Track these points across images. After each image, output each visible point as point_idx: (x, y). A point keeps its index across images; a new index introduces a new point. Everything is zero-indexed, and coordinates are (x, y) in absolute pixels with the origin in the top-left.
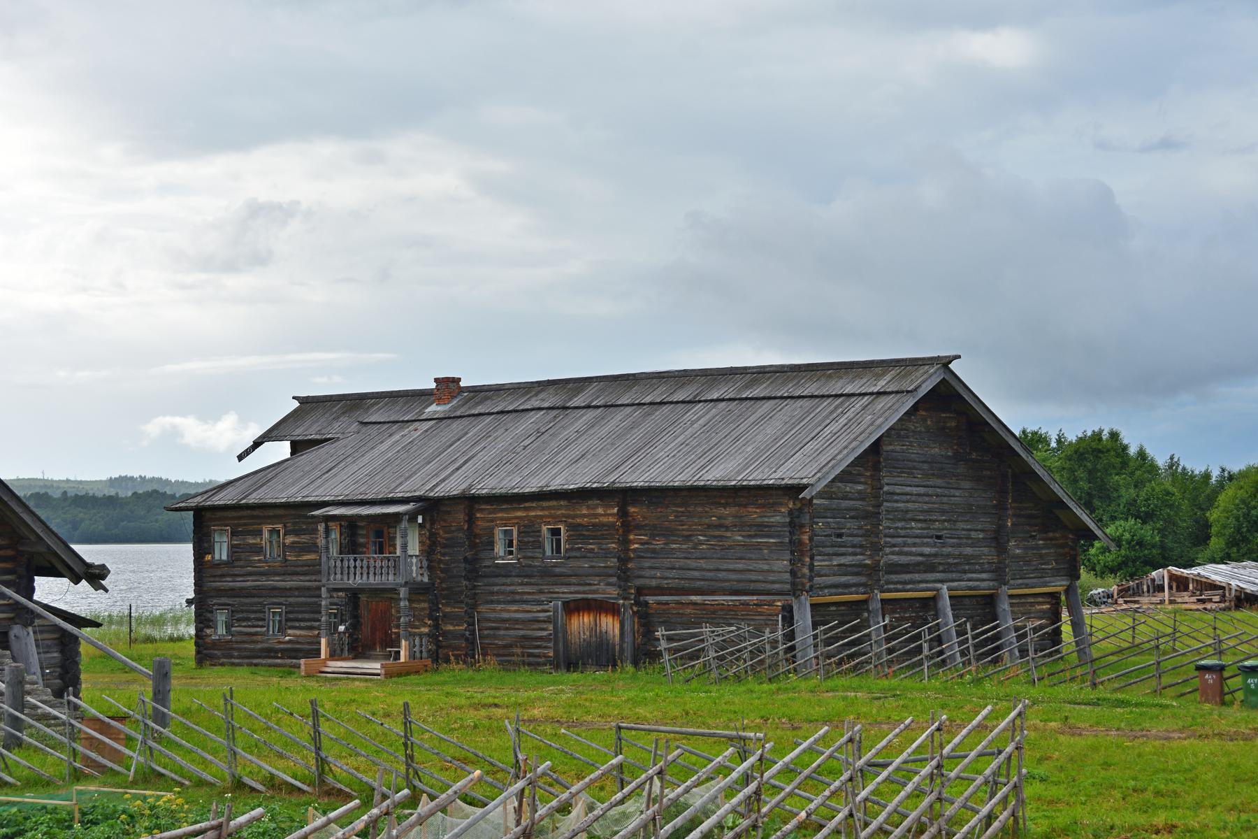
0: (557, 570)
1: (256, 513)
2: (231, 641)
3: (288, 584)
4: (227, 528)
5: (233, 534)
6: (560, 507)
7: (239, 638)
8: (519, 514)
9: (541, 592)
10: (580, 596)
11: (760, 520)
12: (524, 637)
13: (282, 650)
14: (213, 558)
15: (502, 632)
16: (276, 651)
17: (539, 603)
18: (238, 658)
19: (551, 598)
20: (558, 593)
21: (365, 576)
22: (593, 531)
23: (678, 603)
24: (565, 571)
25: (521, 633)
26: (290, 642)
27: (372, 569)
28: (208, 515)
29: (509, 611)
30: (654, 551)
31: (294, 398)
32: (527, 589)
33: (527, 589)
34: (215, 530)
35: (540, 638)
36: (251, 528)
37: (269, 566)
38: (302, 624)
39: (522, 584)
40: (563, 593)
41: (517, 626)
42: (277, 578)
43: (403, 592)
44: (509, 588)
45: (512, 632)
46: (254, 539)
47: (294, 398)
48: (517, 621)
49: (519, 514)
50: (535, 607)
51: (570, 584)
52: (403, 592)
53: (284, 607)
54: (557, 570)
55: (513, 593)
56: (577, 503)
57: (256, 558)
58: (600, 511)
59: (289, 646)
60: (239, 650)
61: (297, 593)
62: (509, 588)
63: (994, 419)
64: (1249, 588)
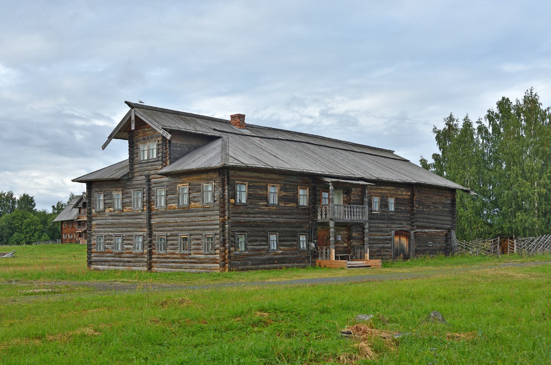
0: (394, 217)
1: (262, 175)
2: (247, 255)
3: (281, 220)
4: (246, 183)
5: (249, 187)
6: (392, 190)
7: (252, 253)
8: (379, 191)
9: (387, 227)
10: (400, 229)
11: (445, 202)
12: (383, 247)
13: (278, 259)
14: (236, 201)
15: (375, 245)
16: (274, 260)
17: (387, 232)
18: (250, 266)
19: (391, 229)
20: (392, 227)
21: (350, 217)
22: (403, 201)
23: (422, 232)
24: (395, 218)
25: (382, 245)
26: (282, 254)
27: (352, 213)
28: (231, 172)
29: (376, 235)
30: (420, 211)
31: (126, 102)
32: (383, 226)
33: (383, 226)
34: (237, 184)
35: (387, 248)
36: (257, 184)
37: (269, 209)
38: (285, 243)
39: (381, 223)
40: (394, 227)
41: (379, 242)
42: (275, 216)
43: (332, 224)
44: (377, 225)
45: (378, 245)
46: (262, 191)
47: (126, 102)
48: (379, 239)
49: (379, 191)
50: (386, 233)
51: (396, 224)
52: (332, 224)
53: (278, 233)
54: (394, 217)
55: (378, 227)
56: (398, 189)
57: (262, 203)
58: (404, 193)
59: (282, 256)
60: (251, 260)
61: (284, 226)
62: (377, 225)
63: (91, 175)
64: (9, 250)
